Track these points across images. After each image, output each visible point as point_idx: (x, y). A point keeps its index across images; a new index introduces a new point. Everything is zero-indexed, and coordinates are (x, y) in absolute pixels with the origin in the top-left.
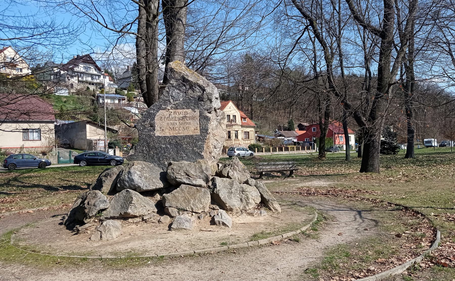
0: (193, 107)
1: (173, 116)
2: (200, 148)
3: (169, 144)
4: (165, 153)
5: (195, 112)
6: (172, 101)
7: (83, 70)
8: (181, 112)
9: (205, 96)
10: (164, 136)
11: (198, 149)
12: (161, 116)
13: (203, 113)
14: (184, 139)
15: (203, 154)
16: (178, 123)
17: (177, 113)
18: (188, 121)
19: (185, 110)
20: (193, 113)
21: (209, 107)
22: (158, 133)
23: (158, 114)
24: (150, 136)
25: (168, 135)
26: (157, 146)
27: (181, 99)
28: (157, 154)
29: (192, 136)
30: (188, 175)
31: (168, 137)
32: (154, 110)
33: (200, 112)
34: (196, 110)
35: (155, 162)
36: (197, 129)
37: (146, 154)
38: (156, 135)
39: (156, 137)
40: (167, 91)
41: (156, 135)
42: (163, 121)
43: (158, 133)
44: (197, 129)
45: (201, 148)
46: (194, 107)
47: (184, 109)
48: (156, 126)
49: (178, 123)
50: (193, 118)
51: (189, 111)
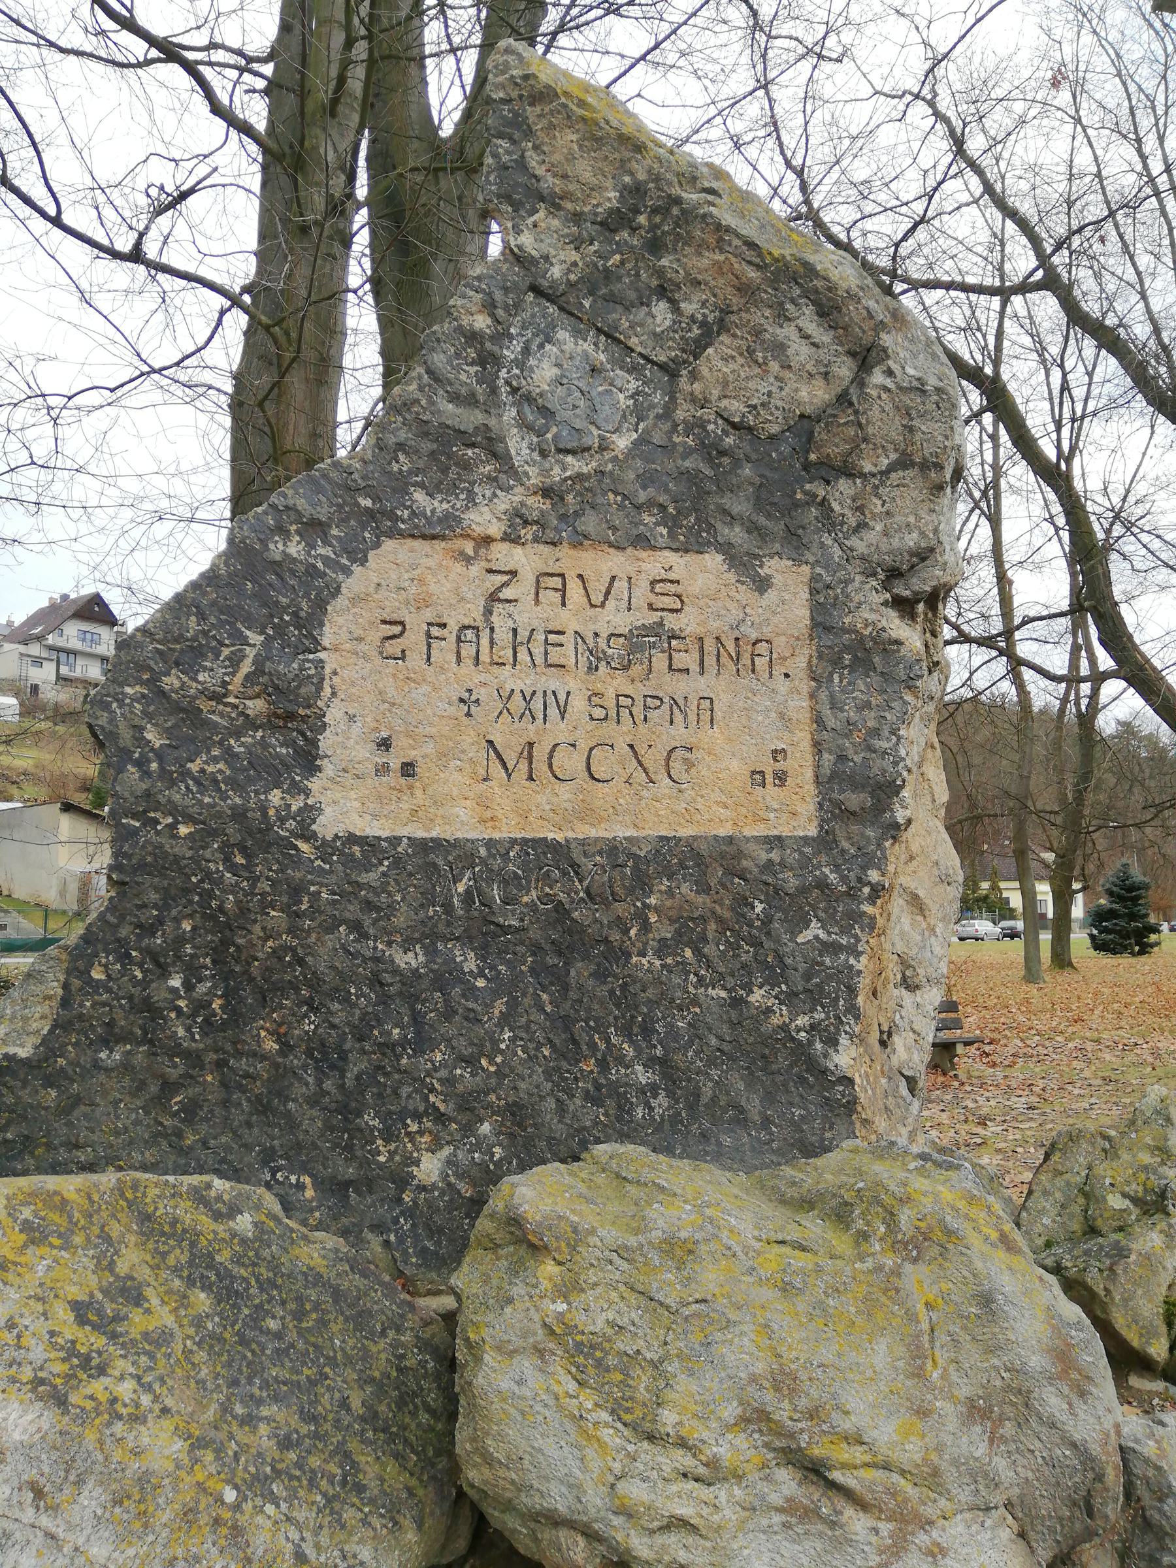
0: (736, 535)
1: (528, 615)
2: (815, 998)
3: (466, 939)
4: (422, 1043)
5: (762, 585)
6: (519, 446)
7: (75, 644)
8: (622, 580)
9: (882, 420)
10: (424, 846)
11: (789, 999)
12: (393, 605)
13: (843, 604)
14: (642, 883)
15: (844, 1058)
16: (578, 704)
17: (575, 590)
18: (680, 686)
19: (654, 564)
20: (745, 593)
21: (911, 540)
22: (346, 803)
23: (357, 581)
24: (257, 838)
25: (460, 822)
26: (326, 951)
27: (622, 442)
28: (329, 1058)
29: (729, 852)
30: (814, 1471)
31: (459, 854)
32: (314, 528)
33: (816, 588)
34: (772, 567)
35: (299, 1155)
36: (781, 778)
37: (194, 1059)
38: (328, 825)
39: (325, 849)
40: (473, 337)
41: (328, 825)
42: (416, 660)
43: (346, 803)
44: (781, 778)
45: (829, 990)
46: (752, 528)
47: (642, 541)
48: (334, 715)
49: (578, 704)
50: (741, 653)
51: (703, 572)
